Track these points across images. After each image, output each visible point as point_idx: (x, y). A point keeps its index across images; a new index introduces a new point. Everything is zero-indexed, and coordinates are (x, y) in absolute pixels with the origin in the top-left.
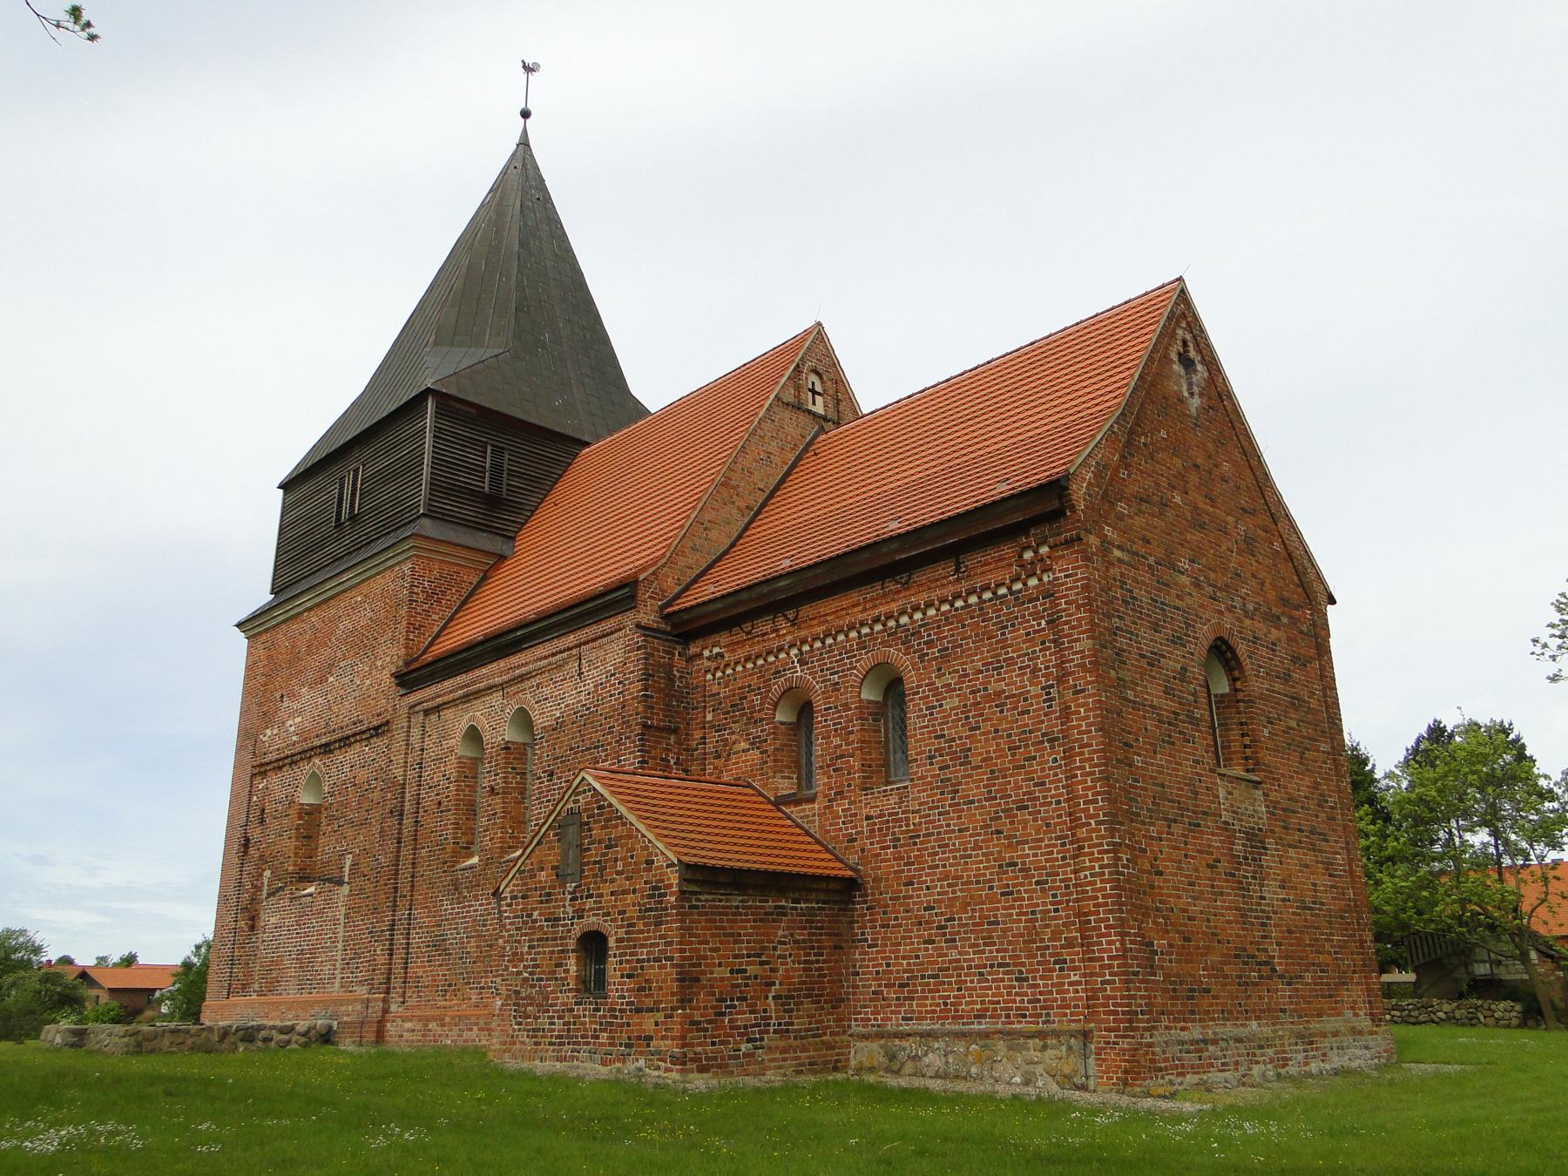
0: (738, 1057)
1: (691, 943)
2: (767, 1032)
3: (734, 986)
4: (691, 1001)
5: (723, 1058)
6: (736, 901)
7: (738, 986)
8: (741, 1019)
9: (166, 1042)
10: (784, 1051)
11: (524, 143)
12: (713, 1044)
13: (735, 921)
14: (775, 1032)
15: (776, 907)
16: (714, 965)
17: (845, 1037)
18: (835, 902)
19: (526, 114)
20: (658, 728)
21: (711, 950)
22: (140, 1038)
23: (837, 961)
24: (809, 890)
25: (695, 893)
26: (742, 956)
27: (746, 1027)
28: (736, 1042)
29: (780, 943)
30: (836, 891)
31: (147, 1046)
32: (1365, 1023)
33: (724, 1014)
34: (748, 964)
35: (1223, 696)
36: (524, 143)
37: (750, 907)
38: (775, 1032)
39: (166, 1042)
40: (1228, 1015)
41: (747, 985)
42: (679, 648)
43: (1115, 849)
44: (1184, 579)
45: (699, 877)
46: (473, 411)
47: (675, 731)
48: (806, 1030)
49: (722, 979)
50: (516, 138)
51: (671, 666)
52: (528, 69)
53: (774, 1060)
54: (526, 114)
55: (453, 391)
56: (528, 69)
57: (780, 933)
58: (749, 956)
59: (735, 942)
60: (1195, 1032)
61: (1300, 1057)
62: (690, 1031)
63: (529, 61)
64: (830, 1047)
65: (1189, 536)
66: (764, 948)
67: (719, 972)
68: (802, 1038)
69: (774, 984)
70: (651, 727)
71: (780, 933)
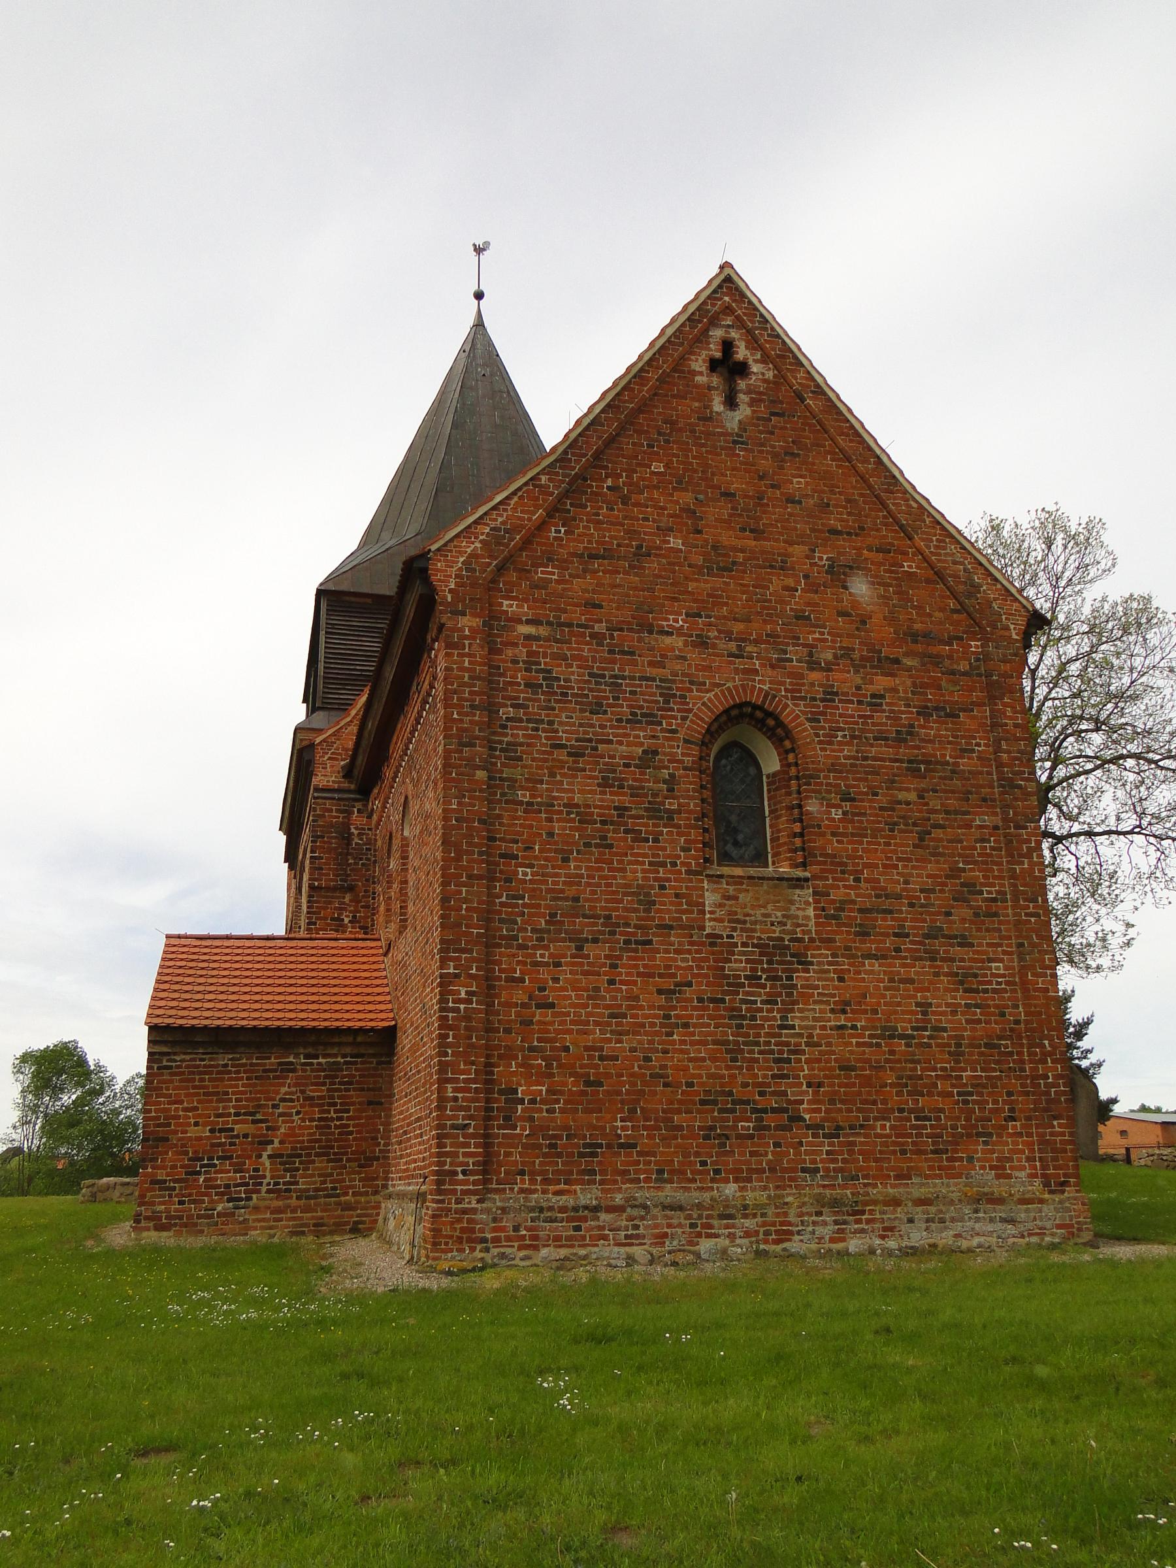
0: (211, 1216)
1: (159, 1103)
2: (259, 1192)
3: (213, 1145)
4: (155, 1160)
5: (190, 1217)
6: (223, 1059)
7: (220, 1145)
8: (221, 1179)
9: (117, 1193)
10: (279, 1210)
11: (479, 324)
12: (181, 1203)
13: (222, 1080)
14: (268, 1191)
15: (280, 1064)
16: (189, 1125)
17: (378, 1198)
18: (374, 1055)
19: (479, 296)
20: (328, 889)
21: (185, 1110)
22: (95, 1189)
23: (368, 1118)
24: (326, 1044)
25: (168, 1054)
26: (229, 1115)
27: (227, 1186)
28: (212, 1201)
29: (283, 1100)
30: (371, 1044)
31: (100, 1196)
32: (1023, 1181)
33: (199, 1173)
34: (235, 1122)
35: (775, 774)
36: (479, 324)
37: (244, 1065)
38: (268, 1191)
39: (117, 1193)
40: (662, 1176)
41: (231, 1144)
42: (359, 805)
43: (445, 982)
44: (677, 642)
45: (166, 1037)
46: (369, 601)
47: (351, 889)
48: (317, 1190)
49: (200, 1139)
50: (471, 321)
51: (346, 826)
52: (479, 250)
53: (263, 1220)
54: (479, 296)
55: (344, 587)
56: (479, 250)
57: (284, 1089)
58: (237, 1114)
59: (220, 1101)
60: (587, 1196)
61: (827, 1231)
62: (148, 1190)
63: (480, 242)
64: (348, 1207)
65: (691, 586)
66: (260, 1106)
67: (192, 1132)
68: (308, 1198)
69: (272, 1142)
70: (319, 888)
71: (284, 1089)
